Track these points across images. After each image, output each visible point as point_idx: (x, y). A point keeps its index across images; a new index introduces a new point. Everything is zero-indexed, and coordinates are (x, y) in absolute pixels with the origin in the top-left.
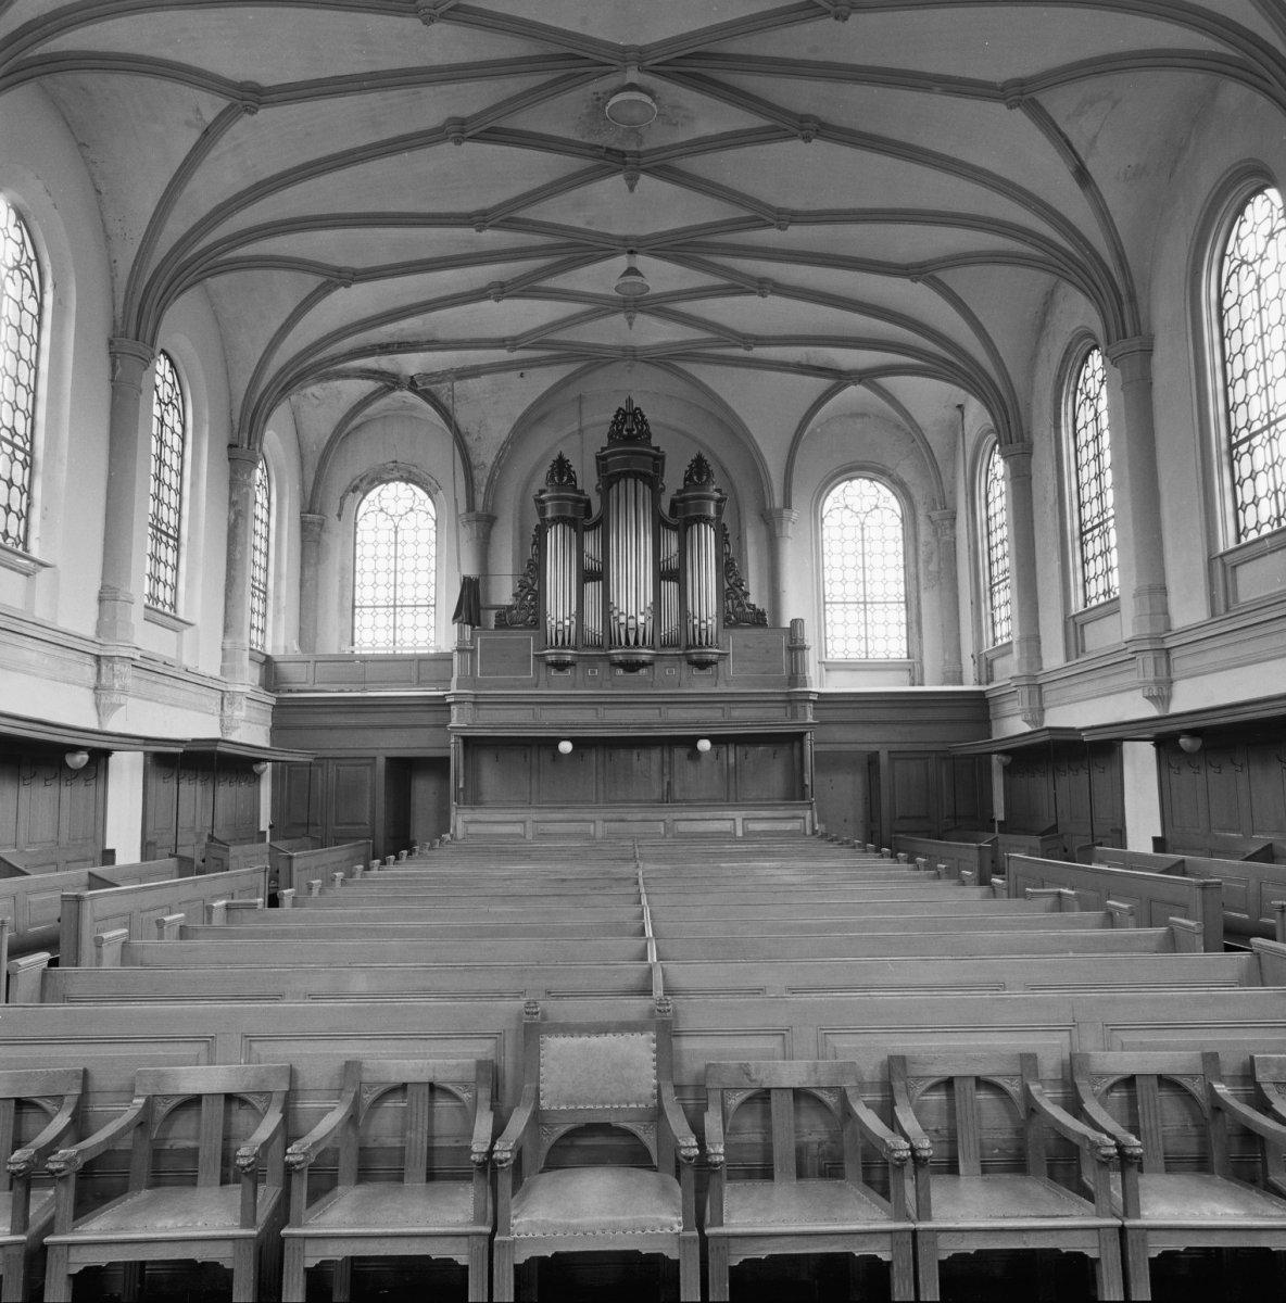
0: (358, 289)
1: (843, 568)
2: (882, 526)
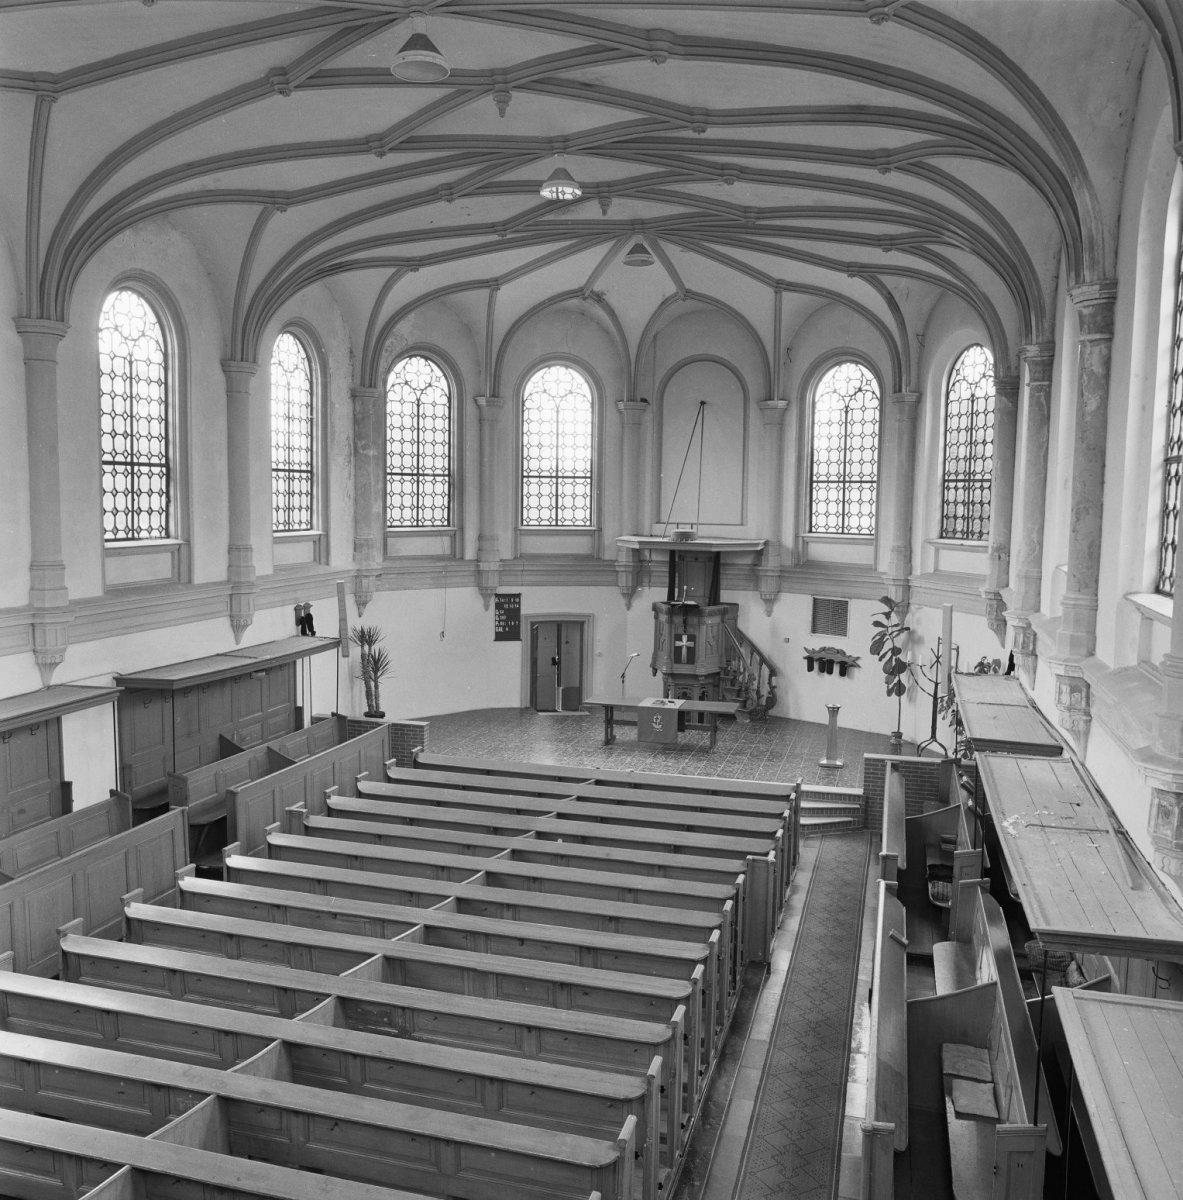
0: (295, 213)
1: (402, 441)
2: (575, 410)
